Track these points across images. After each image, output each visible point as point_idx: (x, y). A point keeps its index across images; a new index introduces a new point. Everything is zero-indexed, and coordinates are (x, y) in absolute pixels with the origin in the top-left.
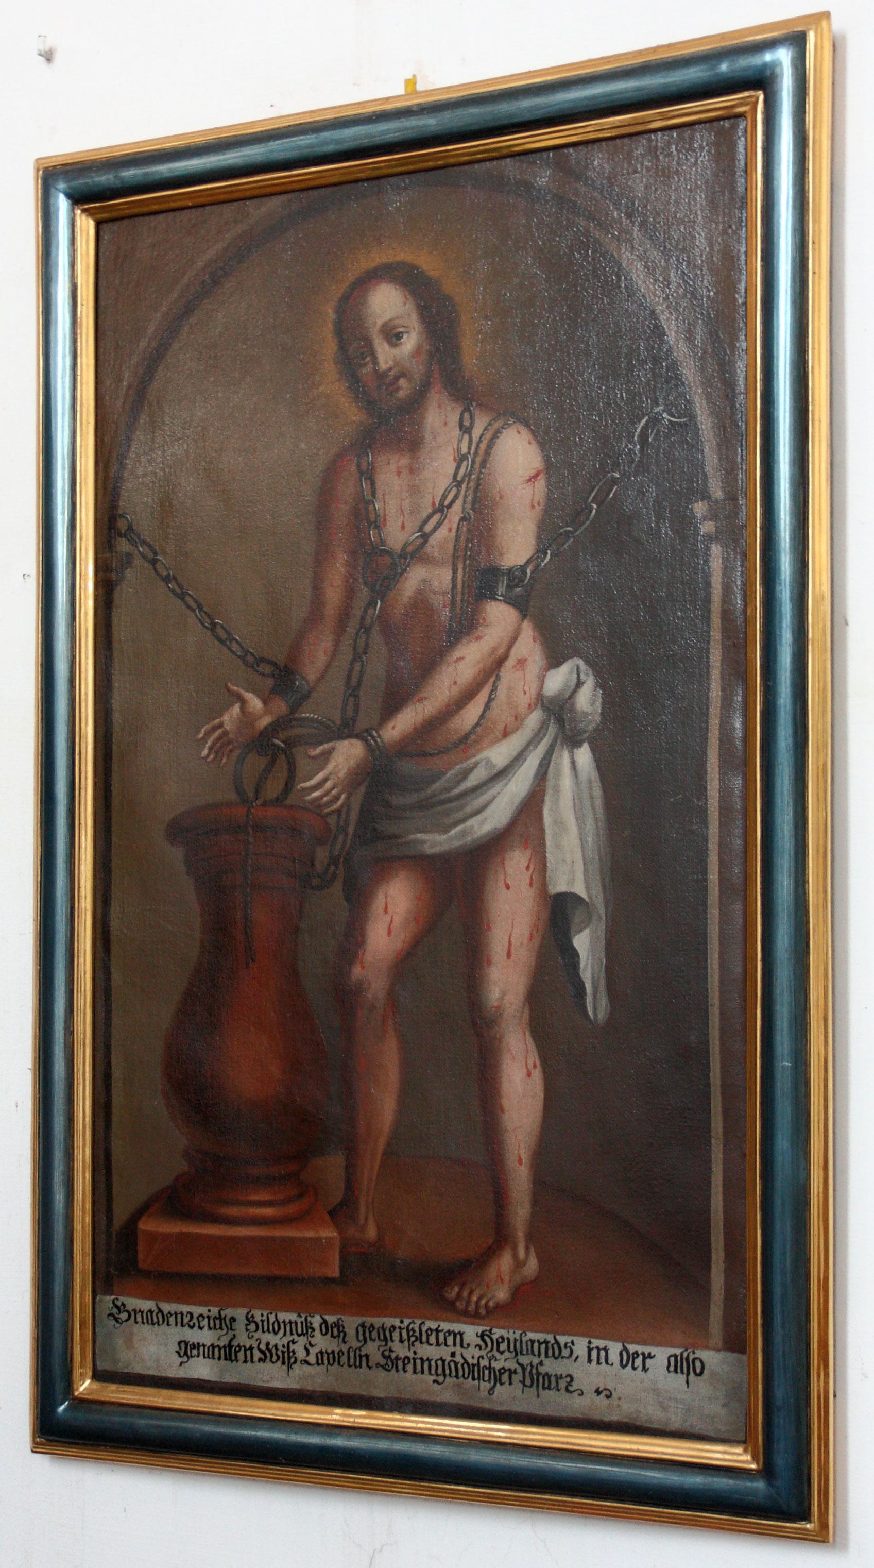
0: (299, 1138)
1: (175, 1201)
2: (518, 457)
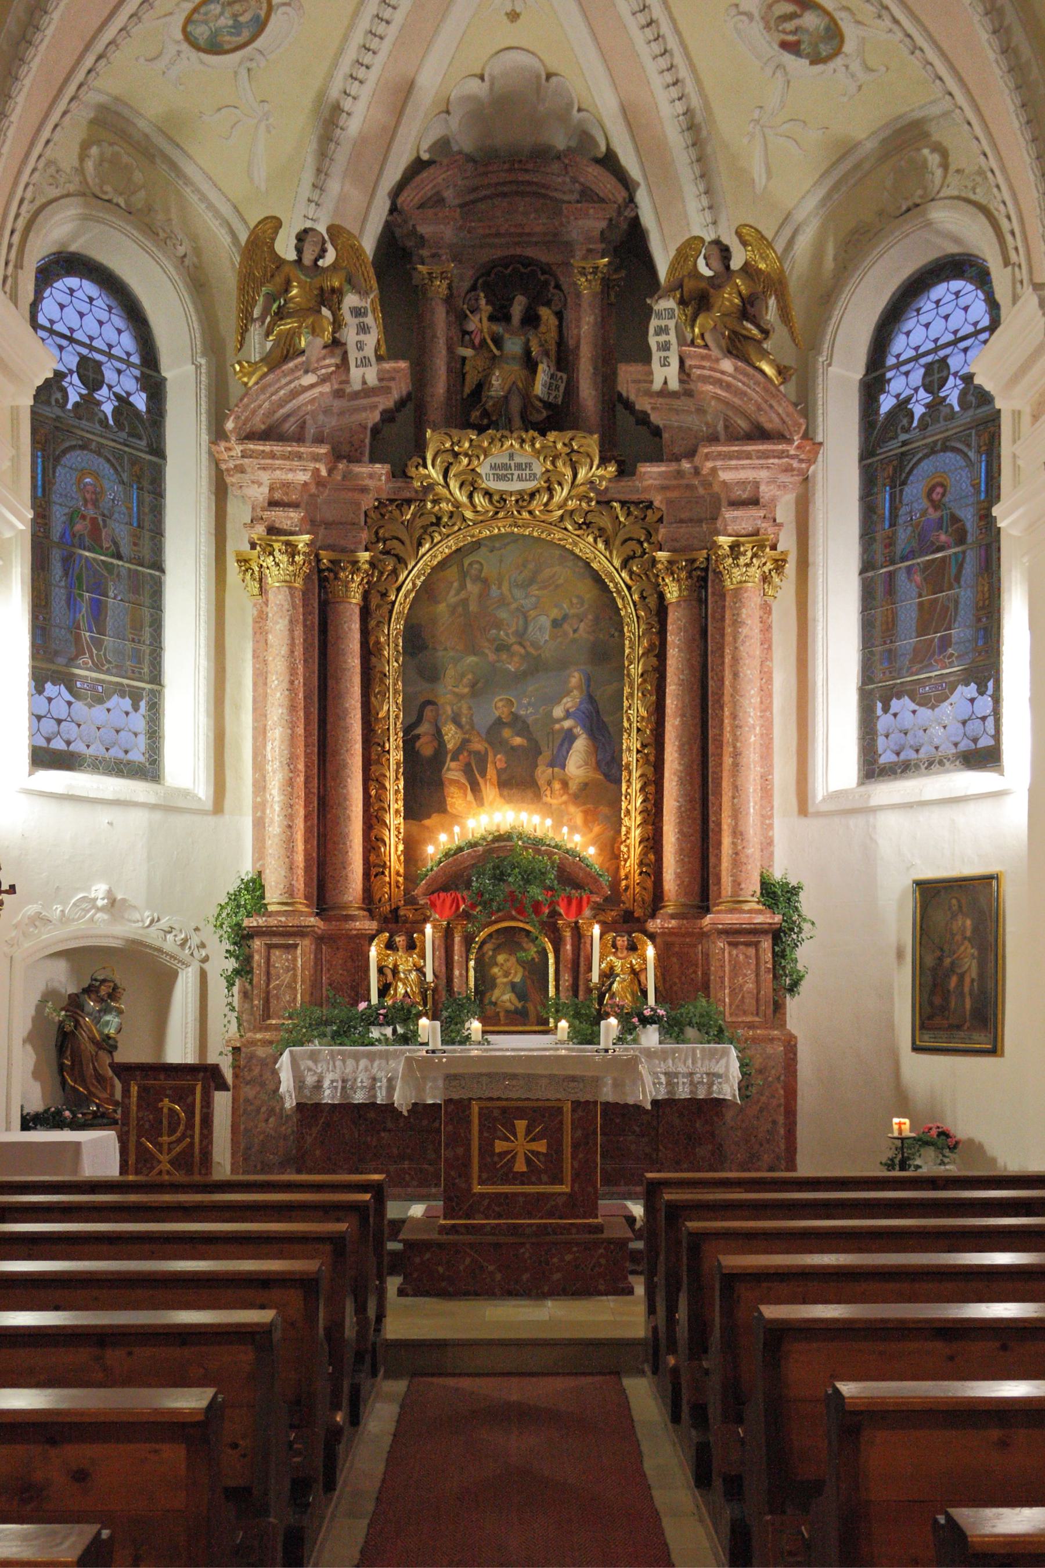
0: (944, 1008)
1: (929, 1018)
2: (968, 922)
